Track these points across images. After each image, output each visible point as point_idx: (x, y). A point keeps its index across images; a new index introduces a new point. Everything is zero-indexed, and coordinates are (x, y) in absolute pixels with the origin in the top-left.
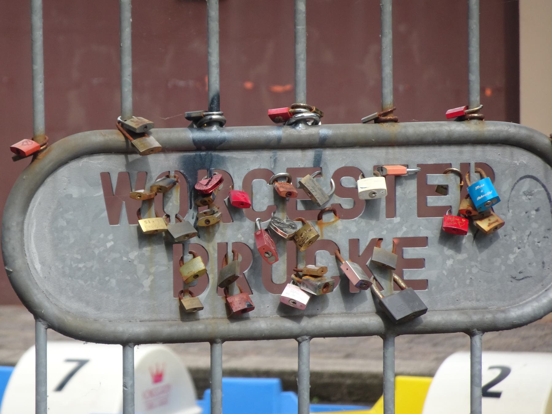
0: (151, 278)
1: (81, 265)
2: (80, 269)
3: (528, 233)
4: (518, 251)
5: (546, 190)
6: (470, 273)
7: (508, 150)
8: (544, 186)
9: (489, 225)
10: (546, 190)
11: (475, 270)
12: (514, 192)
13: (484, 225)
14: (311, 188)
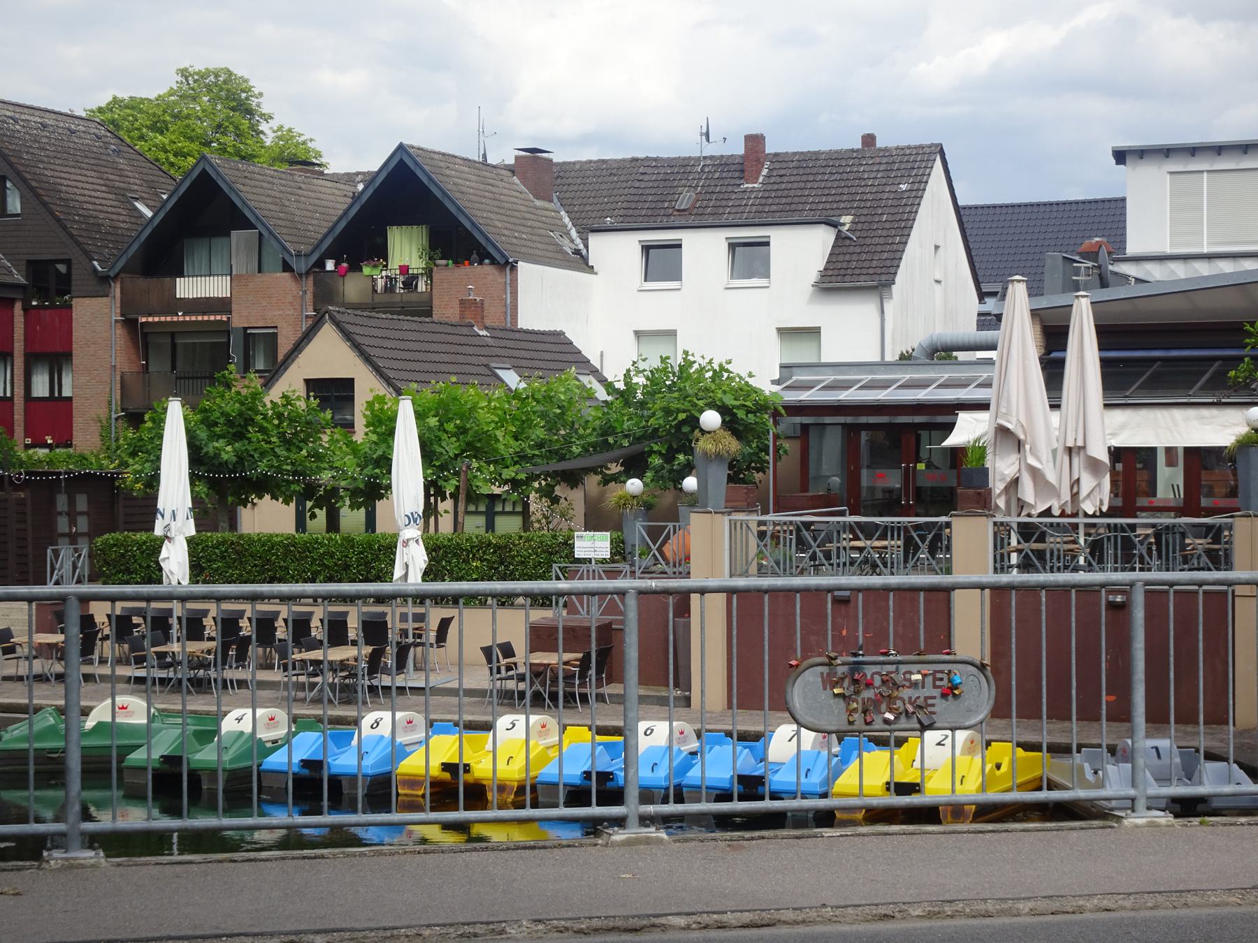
7: (965, 665)
13: (956, 692)
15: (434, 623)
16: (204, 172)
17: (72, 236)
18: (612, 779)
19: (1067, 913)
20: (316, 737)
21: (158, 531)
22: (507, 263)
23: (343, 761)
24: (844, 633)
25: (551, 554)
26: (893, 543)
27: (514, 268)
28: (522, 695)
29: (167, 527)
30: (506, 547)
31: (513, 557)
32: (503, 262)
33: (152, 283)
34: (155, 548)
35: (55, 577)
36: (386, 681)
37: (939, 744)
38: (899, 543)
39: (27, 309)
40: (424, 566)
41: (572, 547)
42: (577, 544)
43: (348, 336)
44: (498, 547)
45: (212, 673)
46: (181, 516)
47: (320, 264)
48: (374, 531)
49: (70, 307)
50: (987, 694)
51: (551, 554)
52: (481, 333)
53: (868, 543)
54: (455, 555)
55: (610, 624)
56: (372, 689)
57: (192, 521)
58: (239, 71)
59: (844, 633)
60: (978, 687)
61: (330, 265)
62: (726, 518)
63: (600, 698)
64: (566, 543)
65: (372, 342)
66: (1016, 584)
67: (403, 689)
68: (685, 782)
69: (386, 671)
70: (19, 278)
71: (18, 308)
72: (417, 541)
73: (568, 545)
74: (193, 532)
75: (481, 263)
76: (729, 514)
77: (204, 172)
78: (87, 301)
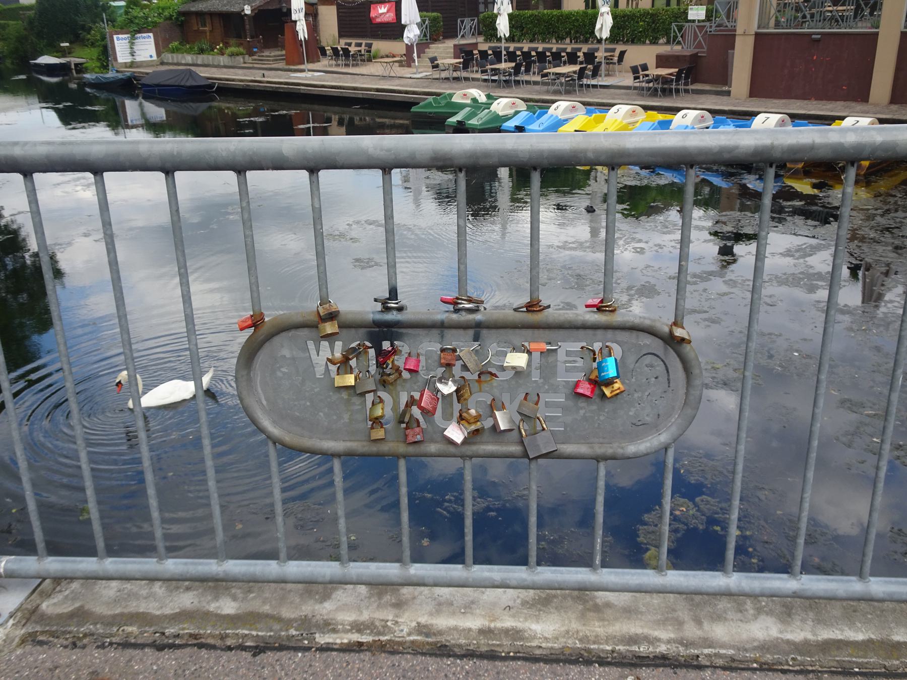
0: (349, 413)
1: (296, 403)
2: (295, 405)
3: (647, 394)
4: (638, 406)
5: (665, 364)
6: (599, 419)
7: (635, 334)
8: (663, 361)
9: (612, 392)
10: (665, 364)
11: (602, 418)
12: (637, 365)
13: (607, 392)
14: (877, 248)
15: (617, 53)
19: (884, 428)
21: (495, 11)
24: (815, 58)
25: (677, 17)
26: (849, 7)
28: (656, 90)
29: (499, 9)
30: (656, 14)
31: (659, 20)
34: (494, 18)
35: (461, 34)
36: (585, 81)
38: (852, 7)
40: (611, 25)
41: (687, 14)
42: (690, 12)
44: (652, 15)
45: (513, 78)
48: (617, 7)
50: (682, 391)
51: (677, 17)
53: (835, 8)
54: (633, 19)
55: (697, 53)
56: (581, 86)
59: (815, 58)
60: (663, 379)
63: (687, 91)
66: (777, 155)
67: (589, 85)
69: (587, 78)
73: (685, 13)
74: (511, 11)
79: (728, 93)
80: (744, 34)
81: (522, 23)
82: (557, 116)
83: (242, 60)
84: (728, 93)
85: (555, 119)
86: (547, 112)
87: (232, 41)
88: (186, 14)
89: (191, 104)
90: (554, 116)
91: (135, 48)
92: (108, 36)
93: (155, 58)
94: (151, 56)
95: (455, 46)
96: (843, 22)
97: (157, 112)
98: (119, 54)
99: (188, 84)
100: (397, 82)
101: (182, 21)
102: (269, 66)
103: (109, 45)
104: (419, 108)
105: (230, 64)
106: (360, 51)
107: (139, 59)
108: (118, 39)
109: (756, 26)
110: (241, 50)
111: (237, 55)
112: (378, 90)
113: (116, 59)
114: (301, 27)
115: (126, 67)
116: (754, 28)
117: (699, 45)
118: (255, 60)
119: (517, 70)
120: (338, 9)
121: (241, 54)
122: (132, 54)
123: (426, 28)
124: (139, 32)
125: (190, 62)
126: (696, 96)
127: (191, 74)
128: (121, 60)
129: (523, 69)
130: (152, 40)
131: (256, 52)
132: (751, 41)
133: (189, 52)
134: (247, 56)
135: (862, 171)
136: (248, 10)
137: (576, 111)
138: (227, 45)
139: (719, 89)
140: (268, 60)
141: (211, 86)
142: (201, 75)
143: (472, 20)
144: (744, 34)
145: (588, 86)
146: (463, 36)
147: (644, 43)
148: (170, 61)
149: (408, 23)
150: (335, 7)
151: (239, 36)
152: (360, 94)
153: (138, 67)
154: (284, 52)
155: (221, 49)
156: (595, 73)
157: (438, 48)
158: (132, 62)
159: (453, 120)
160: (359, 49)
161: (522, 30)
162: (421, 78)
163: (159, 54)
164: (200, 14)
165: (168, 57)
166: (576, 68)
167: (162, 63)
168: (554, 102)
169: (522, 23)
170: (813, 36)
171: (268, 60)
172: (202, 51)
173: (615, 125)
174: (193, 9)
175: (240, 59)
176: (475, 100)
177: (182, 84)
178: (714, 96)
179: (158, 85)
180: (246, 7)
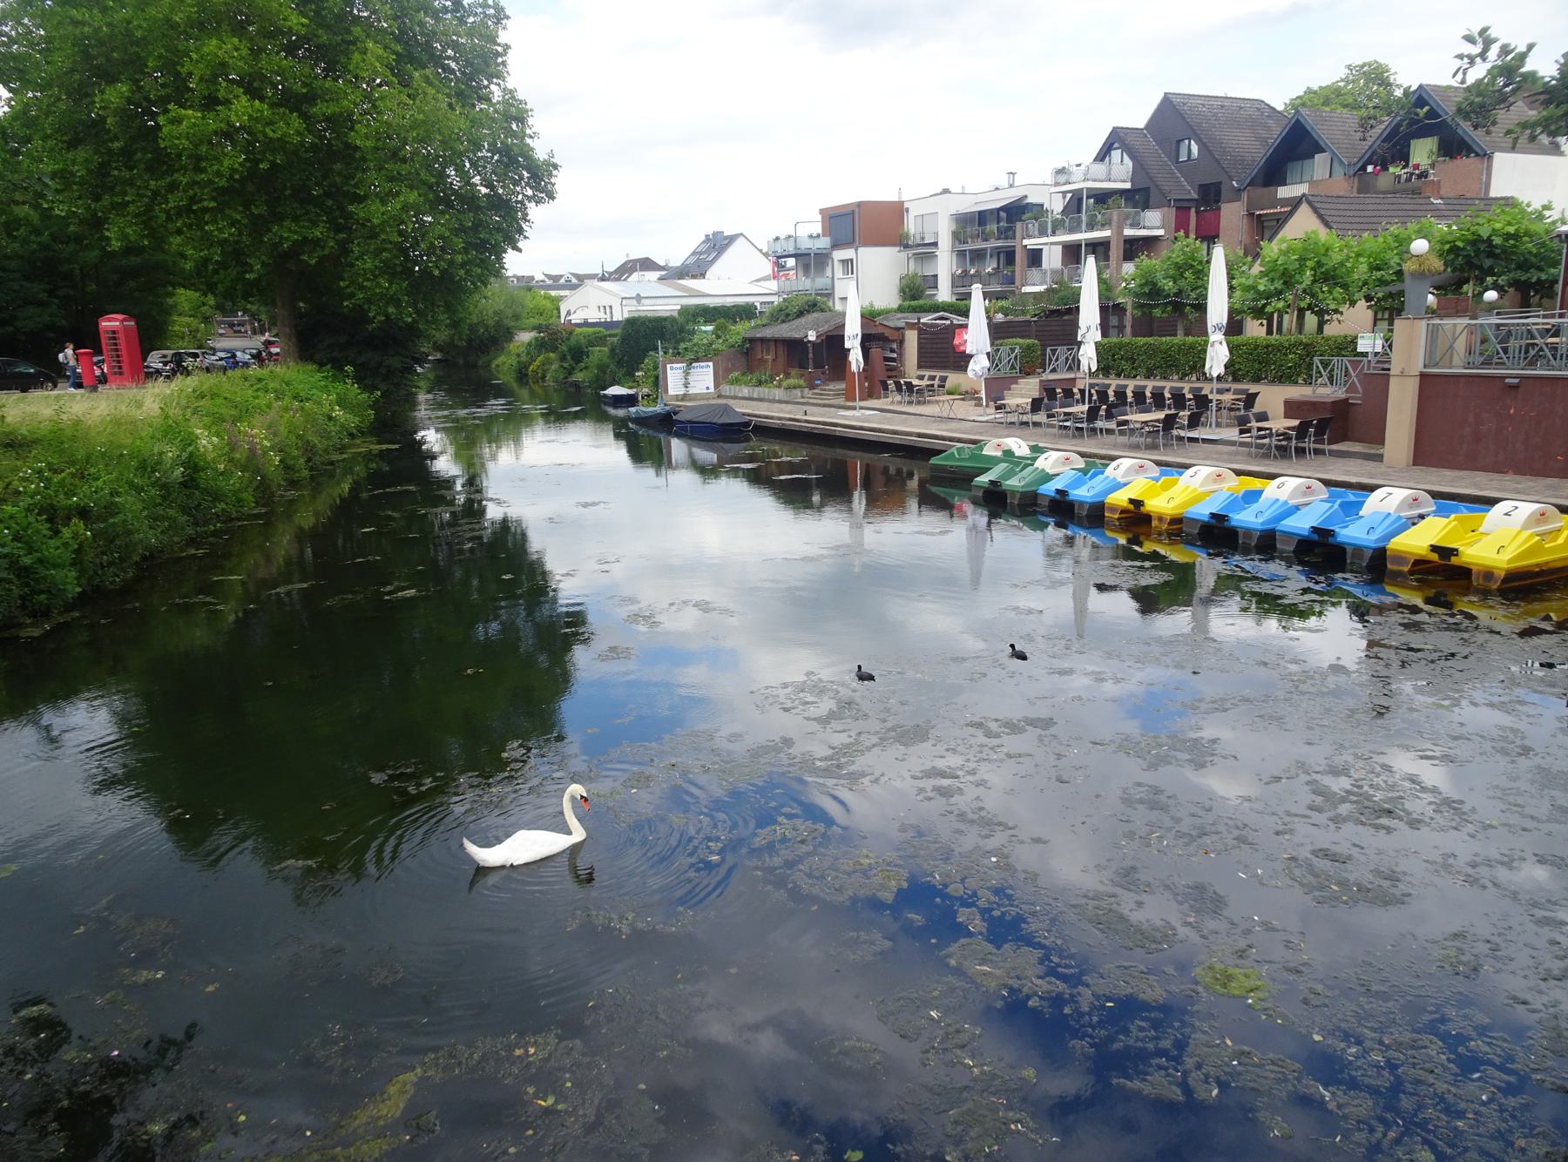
16: (1298, 120)
17: (1223, 168)
18: (1457, 555)
20: (1443, 525)
22: (1485, 154)
23: (1353, 533)
24: (1512, 411)
27: (1490, 158)
32: (1482, 153)
33: (1266, 190)
37: (1506, 514)
39: (1197, 212)
43: (1315, 210)
44: (1307, 345)
46: (1093, 328)
47: (1363, 168)
48: (1322, 333)
49: (1219, 209)
52: (1435, 202)
54: (1279, 350)
55: (1348, 399)
57: (1099, 332)
58: (1382, 61)
59: (1512, 411)
61: (1370, 169)
62: (1424, 323)
63: (1317, 452)
64: (1352, 342)
65: (1329, 213)
68: (1279, 528)
70: (1195, 196)
71: (1193, 210)
72: (1221, 343)
75: (1467, 157)
76: (1429, 319)
77: (1298, 120)
78: (1228, 205)
79: (1379, 458)
80: (1402, 374)
81: (1133, 353)
82: (1115, 479)
83: (799, 394)
84: (1379, 458)
85: (1112, 481)
86: (1102, 473)
87: (794, 372)
88: (752, 341)
89: (721, 444)
90: (1111, 477)
91: (690, 378)
92: (660, 366)
93: (712, 390)
94: (708, 388)
95: (1041, 381)
96: (1555, 359)
97: (708, 456)
98: (670, 385)
99: (720, 422)
100: (954, 425)
101: (747, 349)
102: (826, 402)
103: (661, 376)
104: (941, 459)
105: (785, 399)
106: (932, 386)
107: (692, 391)
108: (672, 369)
109: (1421, 364)
110: (802, 382)
111: (795, 388)
112: (920, 435)
113: (666, 391)
114: (854, 357)
115: (678, 400)
116: (1418, 366)
117: (1352, 389)
118: (816, 394)
119: (1092, 414)
120: (919, 335)
121: (800, 387)
122: (686, 385)
123: (1050, 360)
124: (697, 360)
125: (747, 395)
126: (1333, 459)
127: (727, 408)
128: (671, 392)
129: (1102, 413)
130: (711, 369)
131: (818, 385)
132: (1413, 386)
133: (746, 384)
134: (806, 390)
135: (1496, 583)
136: (812, 336)
137: (1312, 494)
138: (787, 375)
139: (1373, 451)
140: (828, 395)
141: (747, 424)
142: (737, 410)
143: (1068, 349)
144: (1402, 374)
145: (1180, 439)
146: (1054, 370)
147: (1296, 383)
148: (728, 394)
149: (974, 352)
150: (916, 332)
151: (803, 366)
152: (897, 439)
153: (690, 400)
154: (843, 386)
155: (781, 380)
156: (1194, 422)
157: (1028, 384)
158: (685, 395)
159: (984, 479)
160: (932, 382)
161: (1133, 363)
162: (987, 422)
163: (717, 385)
164: (763, 340)
165: (726, 389)
166: (1161, 415)
167: (719, 396)
168: (1113, 458)
169: (1133, 353)
170: (1507, 380)
171: (828, 395)
172: (760, 383)
173: (1273, 509)
174: (758, 335)
175: (798, 392)
176: (1008, 453)
177: (714, 421)
178: (1360, 461)
179: (690, 422)
180: (810, 333)
